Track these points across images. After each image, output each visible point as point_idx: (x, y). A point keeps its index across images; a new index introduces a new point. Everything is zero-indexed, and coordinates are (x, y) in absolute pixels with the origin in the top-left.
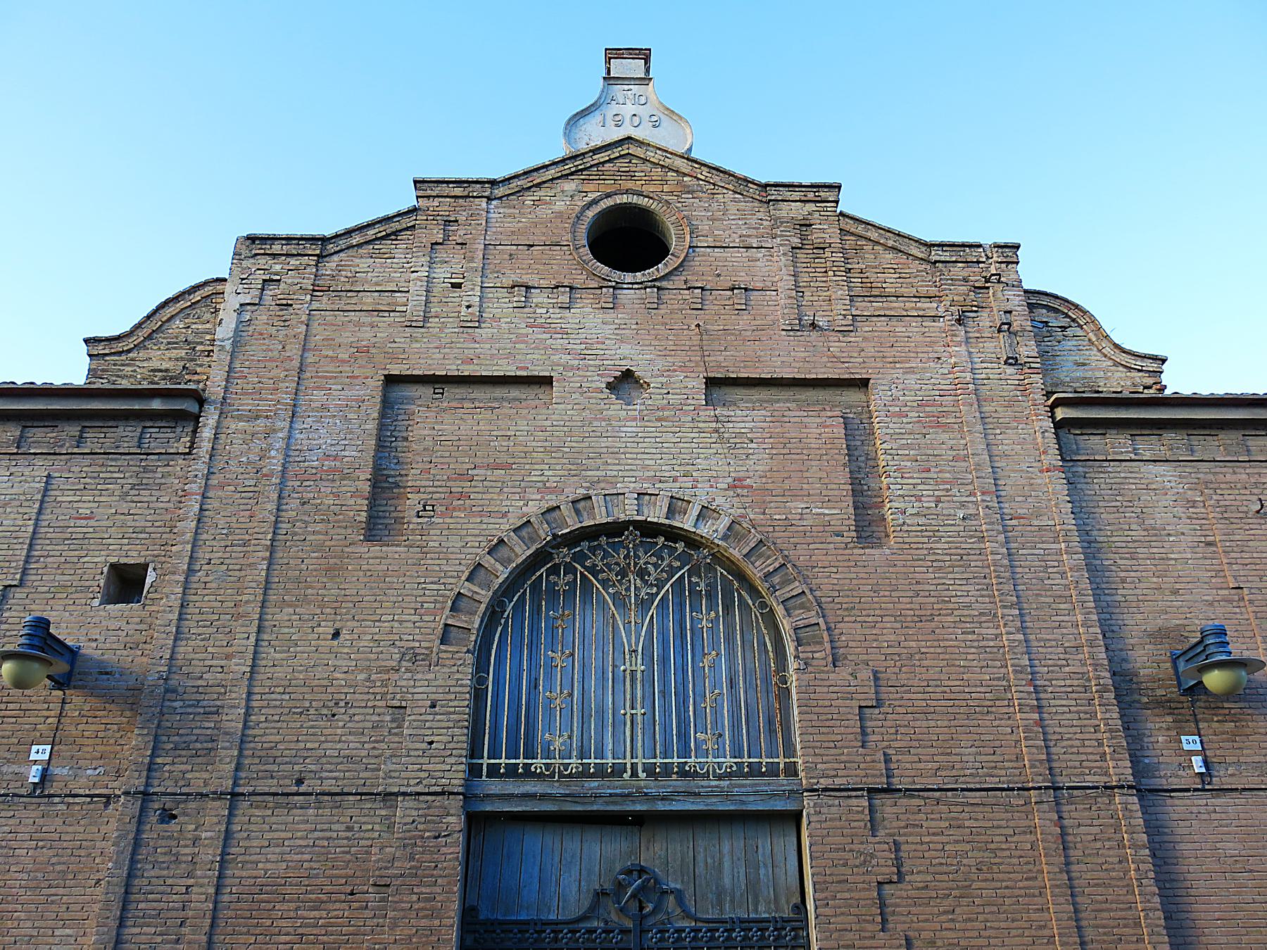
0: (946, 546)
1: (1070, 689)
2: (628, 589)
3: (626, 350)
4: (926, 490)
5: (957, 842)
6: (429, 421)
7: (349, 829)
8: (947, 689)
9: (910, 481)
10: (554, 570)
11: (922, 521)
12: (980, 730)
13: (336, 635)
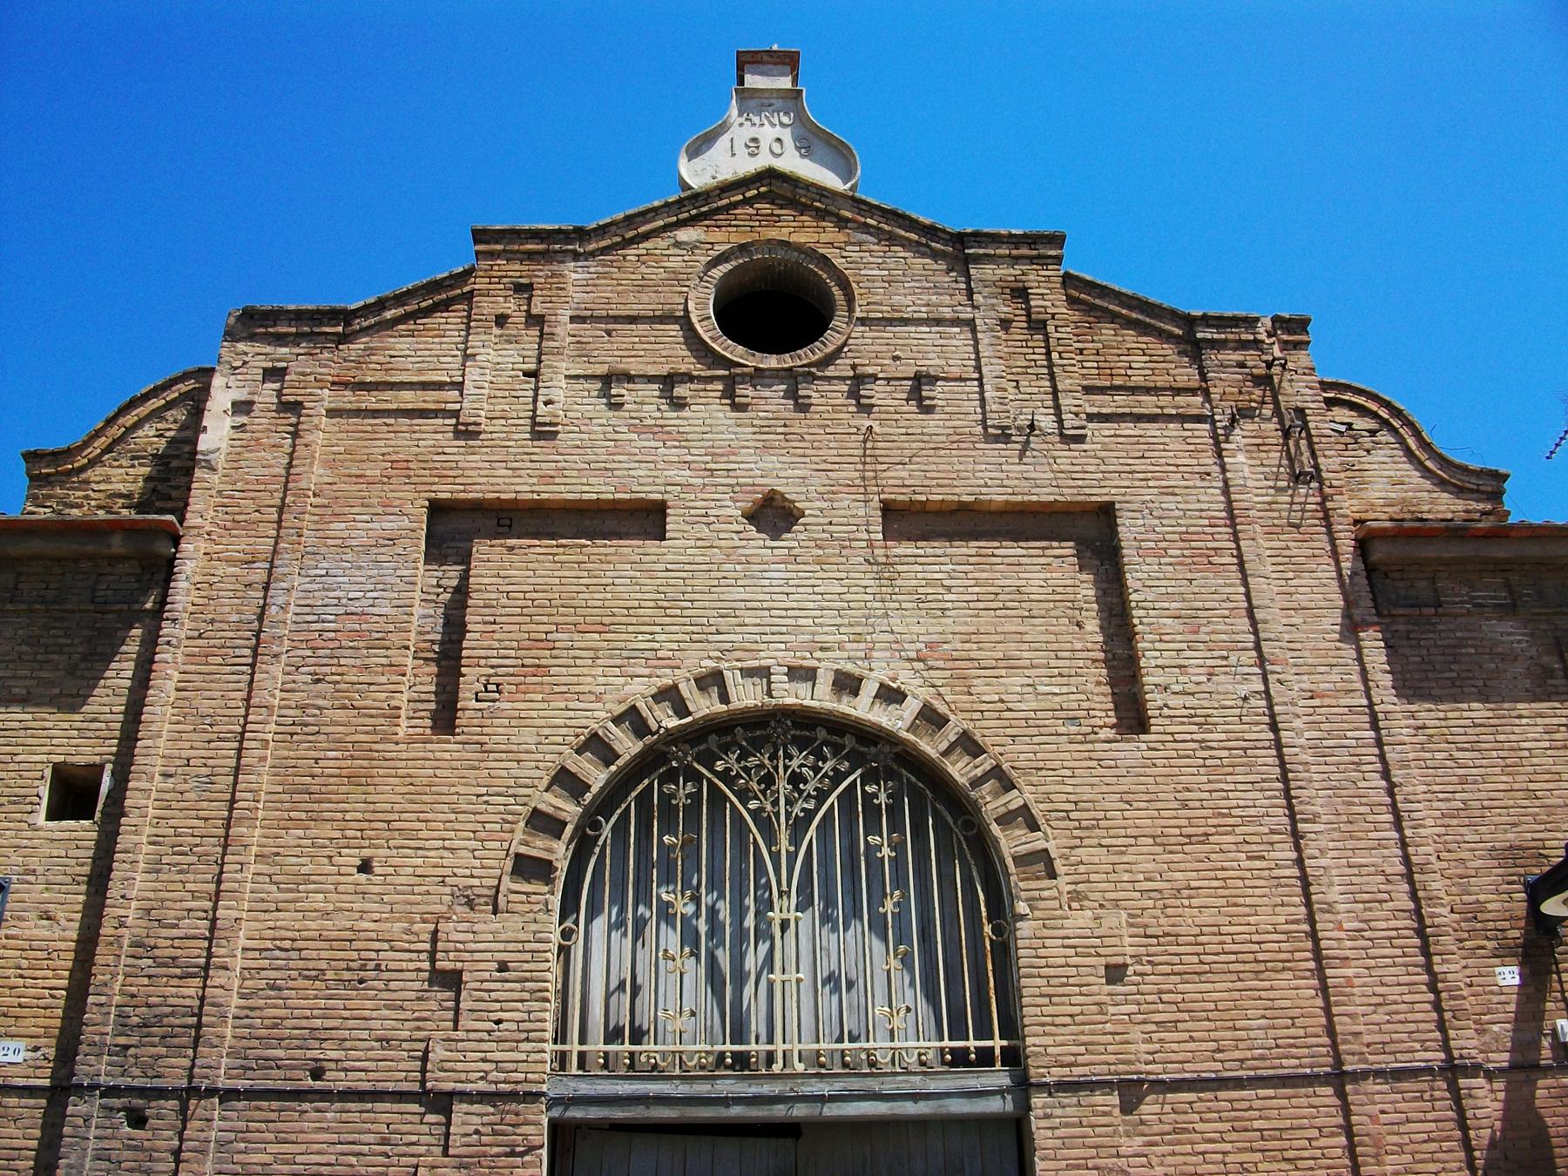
0: (1223, 736)
1: (1394, 933)
2: (775, 803)
3: (771, 461)
4: (1194, 658)
5: (1240, 1150)
6: (497, 565)
7: (384, 1142)
8: (1228, 939)
9: (1172, 646)
10: (670, 776)
11: (1190, 701)
12: (1272, 994)
13: (365, 867)
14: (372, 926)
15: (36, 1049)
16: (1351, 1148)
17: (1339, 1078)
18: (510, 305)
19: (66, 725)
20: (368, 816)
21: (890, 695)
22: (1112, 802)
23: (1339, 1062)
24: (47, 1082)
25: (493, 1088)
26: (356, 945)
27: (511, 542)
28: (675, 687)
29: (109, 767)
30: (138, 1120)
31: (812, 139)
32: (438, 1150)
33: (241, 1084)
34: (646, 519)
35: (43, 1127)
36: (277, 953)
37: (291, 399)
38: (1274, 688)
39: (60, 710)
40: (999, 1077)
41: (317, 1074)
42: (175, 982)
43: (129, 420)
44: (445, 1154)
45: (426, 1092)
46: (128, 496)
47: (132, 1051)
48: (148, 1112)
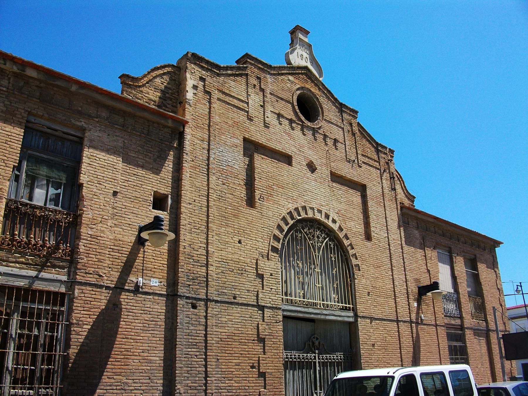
2: (315, 242)
10: (296, 231)
13: (240, 242)
14: (243, 259)
15: (161, 282)
16: (399, 335)
17: (398, 321)
18: (256, 82)
19: (156, 179)
20: (239, 227)
21: (334, 221)
22: (367, 256)
23: (397, 318)
24: (165, 293)
25: (271, 306)
26: (240, 263)
27: (263, 156)
28: (298, 208)
29: (170, 196)
30: (194, 307)
31: (314, 61)
32: (262, 320)
33: (219, 299)
34: (287, 159)
35: (166, 306)
36: (223, 263)
37: (208, 90)
38: (389, 237)
39: (153, 173)
40: (351, 314)
41: (235, 298)
42: (199, 267)
43: (154, 74)
44: (263, 321)
45: (259, 305)
46: (155, 102)
47: (191, 286)
48: (197, 305)
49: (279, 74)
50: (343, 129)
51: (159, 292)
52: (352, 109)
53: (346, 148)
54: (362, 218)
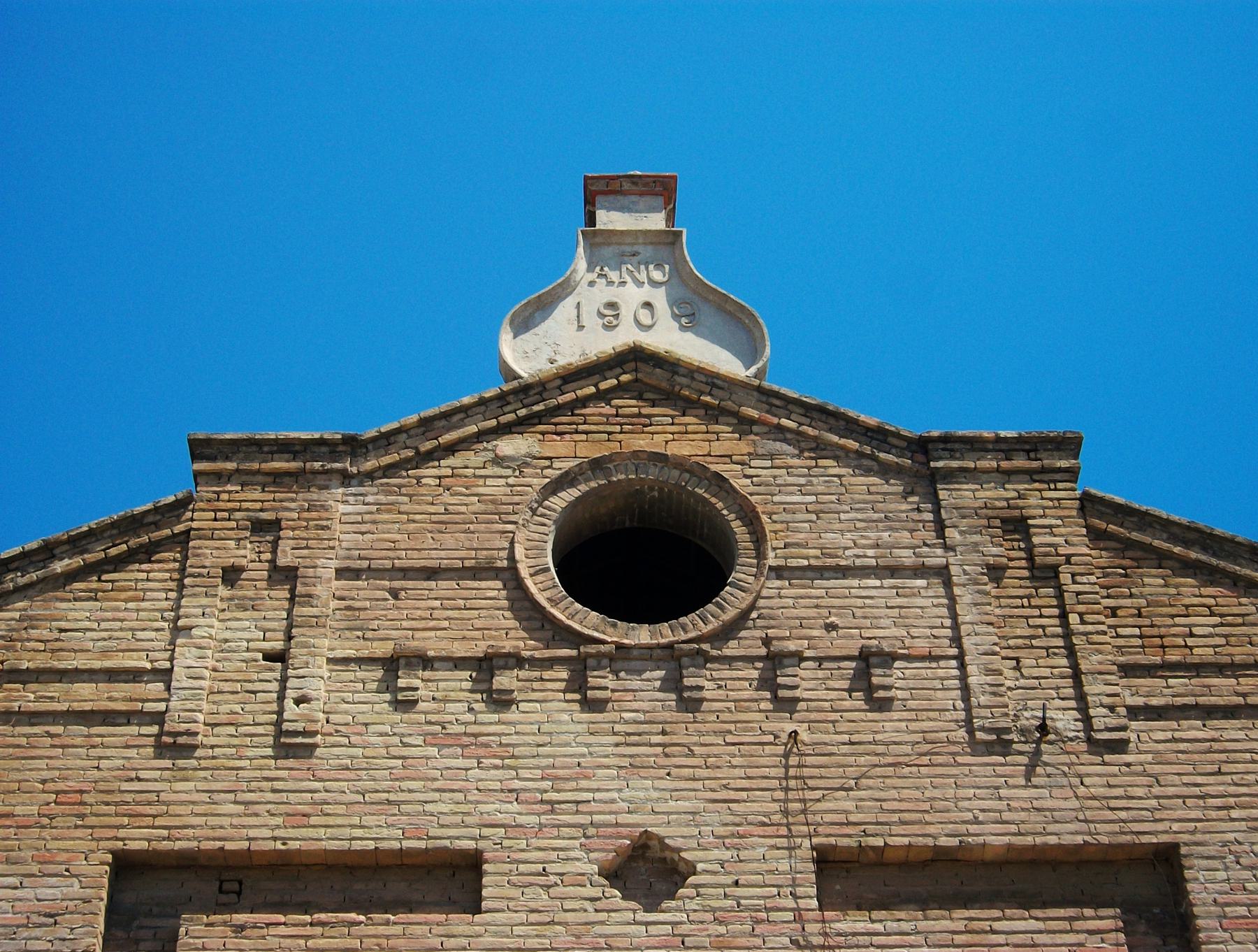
31: (697, 304)
49: (424, 458)
50: (943, 573)
51: (97, 664)
52: (1020, 440)
53: (964, 677)
54: (513, 623)
